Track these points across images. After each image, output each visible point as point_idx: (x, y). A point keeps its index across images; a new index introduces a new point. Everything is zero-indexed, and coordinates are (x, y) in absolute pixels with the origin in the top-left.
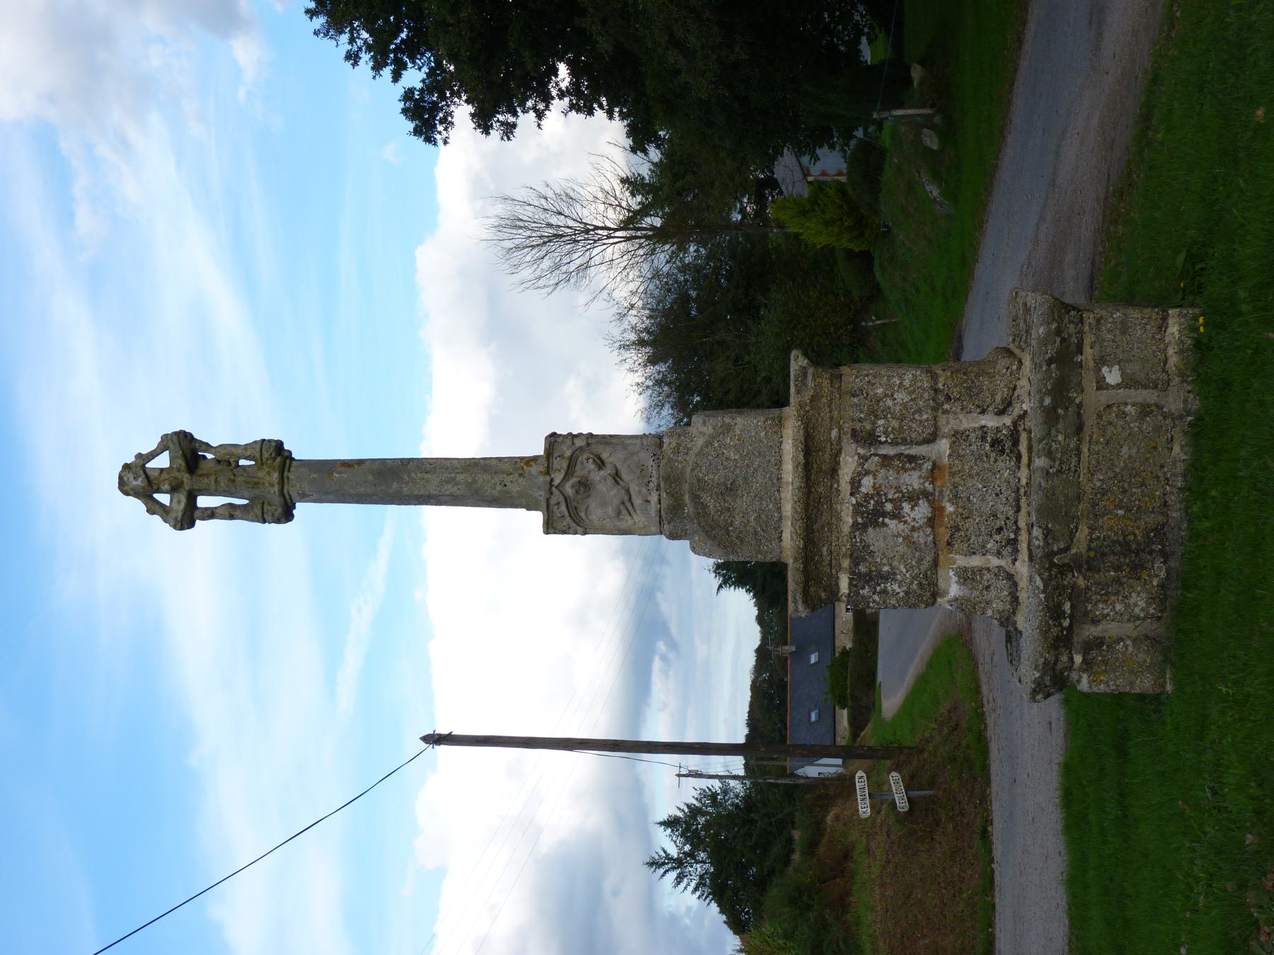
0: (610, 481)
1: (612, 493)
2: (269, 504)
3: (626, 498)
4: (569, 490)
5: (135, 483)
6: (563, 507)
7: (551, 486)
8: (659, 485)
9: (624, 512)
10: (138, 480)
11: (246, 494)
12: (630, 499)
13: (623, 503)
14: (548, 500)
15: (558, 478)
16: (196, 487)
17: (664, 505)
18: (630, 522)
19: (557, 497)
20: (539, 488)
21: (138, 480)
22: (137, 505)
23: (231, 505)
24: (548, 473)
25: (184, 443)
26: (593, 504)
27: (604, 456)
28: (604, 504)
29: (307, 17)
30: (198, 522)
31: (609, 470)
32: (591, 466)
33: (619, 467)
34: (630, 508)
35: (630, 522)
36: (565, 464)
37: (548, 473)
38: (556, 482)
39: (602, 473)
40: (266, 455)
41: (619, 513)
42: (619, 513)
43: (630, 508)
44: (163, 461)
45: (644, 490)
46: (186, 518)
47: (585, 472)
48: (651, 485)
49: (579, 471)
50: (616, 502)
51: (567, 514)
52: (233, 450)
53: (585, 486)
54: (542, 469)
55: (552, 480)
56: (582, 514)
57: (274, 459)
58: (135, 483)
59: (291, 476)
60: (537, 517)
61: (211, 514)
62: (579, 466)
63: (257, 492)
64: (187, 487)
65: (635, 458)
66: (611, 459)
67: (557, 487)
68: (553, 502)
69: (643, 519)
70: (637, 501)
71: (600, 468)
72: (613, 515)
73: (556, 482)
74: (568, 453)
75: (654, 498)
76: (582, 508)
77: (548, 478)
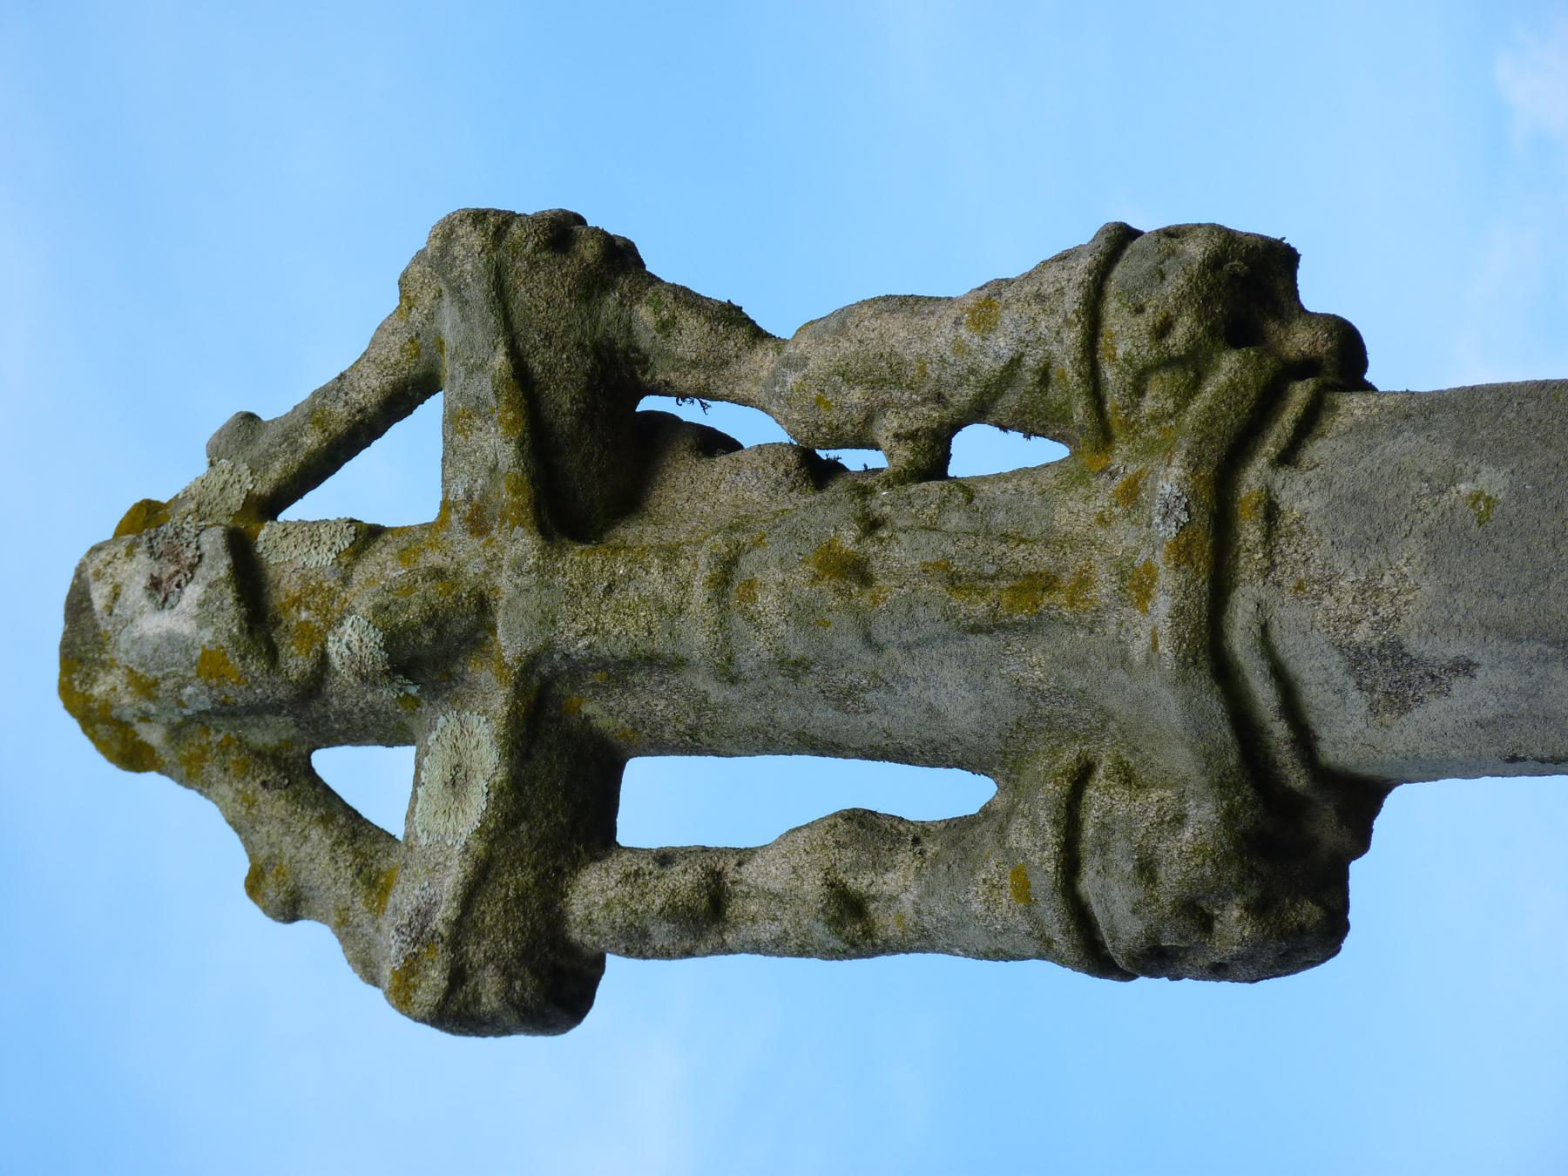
2: (1126, 776)
5: (154, 624)
10: (227, 663)
11: (951, 690)
16: (574, 638)
21: (227, 663)
22: (188, 834)
23: (865, 828)
25: (540, 292)
30: (621, 977)
40: (1125, 336)
44: (399, 480)
46: (516, 956)
52: (897, 330)
57: (1194, 365)
58: (154, 624)
59: (1299, 496)
61: (704, 907)
63: (1032, 663)
64: (510, 641)
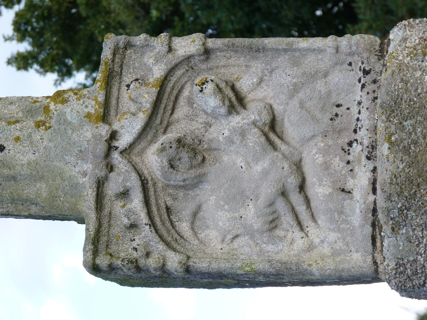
0: (255, 138)
1: (258, 168)
3: (292, 182)
4: (153, 160)
6: (136, 202)
7: (110, 148)
8: (373, 147)
9: (287, 219)
12: (302, 188)
13: (284, 194)
14: (100, 185)
15: (128, 130)
17: (383, 177)
18: (300, 243)
19: (123, 176)
20: (82, 155)
24: (105, 118)
26: (210, 197)
27: (245, 84)
28: (237, 197)
29: (2, 40)
31: (253, 114)
32: (211, 101)
33: (278, 108)
34: (301, 209)
35: (300, 243)
36: (147, 98)
37: (105, 118)
38: (123, 142)
39: (236, 120)
41: (273, 224)
42: (273, 224)
43: (301, 209)
45: (337, 163)
47: (196, 126)
48: (356, 148)
49: (183, 124)
50: (268, 190)
51: (143, 218)
53: (193, 153)
54: (92, 107)
55: (113, 136)
56: (184, 227)
60: (72, 237)
62: (182, 110)
65: (320, 86)
66: (260, 93)
67: (126, 152)
68: (112, 188)
69: (333, 236)
70: (319, 190)
71: (232, 109)
72: (257, 224)
73: (123, 142)
74: (158, 72)
75: (361, 180)
76: (184, 210)
77: (104, 130)
